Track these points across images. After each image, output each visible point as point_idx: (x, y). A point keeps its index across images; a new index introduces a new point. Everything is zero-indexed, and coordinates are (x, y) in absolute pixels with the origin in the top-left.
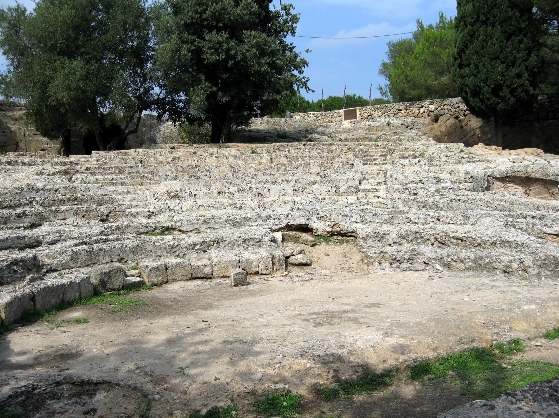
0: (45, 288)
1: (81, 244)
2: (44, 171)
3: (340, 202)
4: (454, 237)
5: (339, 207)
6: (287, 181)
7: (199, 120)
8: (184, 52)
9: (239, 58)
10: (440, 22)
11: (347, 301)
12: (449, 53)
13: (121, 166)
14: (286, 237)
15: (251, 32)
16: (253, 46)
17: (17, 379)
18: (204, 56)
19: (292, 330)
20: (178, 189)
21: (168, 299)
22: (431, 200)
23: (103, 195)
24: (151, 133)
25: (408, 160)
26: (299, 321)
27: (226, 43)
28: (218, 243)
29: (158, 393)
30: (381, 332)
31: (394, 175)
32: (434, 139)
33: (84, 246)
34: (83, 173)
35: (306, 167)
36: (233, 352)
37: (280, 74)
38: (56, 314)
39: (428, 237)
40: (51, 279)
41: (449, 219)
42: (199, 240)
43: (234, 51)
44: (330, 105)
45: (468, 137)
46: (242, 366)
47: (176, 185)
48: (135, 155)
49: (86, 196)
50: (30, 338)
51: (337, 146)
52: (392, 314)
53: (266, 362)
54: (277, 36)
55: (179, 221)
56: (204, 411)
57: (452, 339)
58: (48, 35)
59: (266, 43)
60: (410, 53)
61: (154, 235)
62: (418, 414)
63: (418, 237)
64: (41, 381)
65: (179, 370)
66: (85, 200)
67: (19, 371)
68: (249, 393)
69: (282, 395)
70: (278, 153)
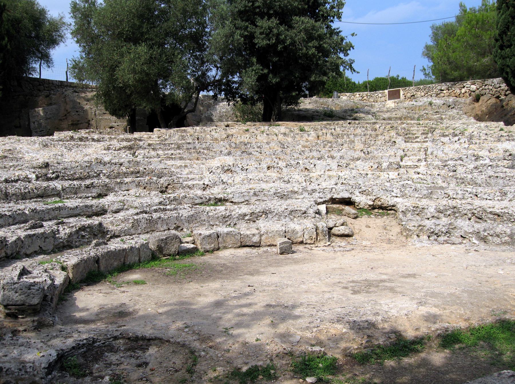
0: (108, 252)
1: (142, 212)
2: (111, 147)
3: (382, 178)
4: (491, 213)
5: (380, 182)
6: (333, 157)
7: (252, 100)
8: (237, 37)
9: (288, 42)
10: (483, 5)
11: (385, 271)
12: (491, 35)
13: (180, 142)
14: (330, 210)
15: (300, 17)
16: (301, 31)
17: (80, 332)
18: (256, 41)
19: (330, 297)
20: (231, 164)
21: (219, 264)
22: (470, 176)
23: (162, 169)
24: (209, 112)
25: (448, 138)
26: (338, 289)
27: (276, 28)
28: (266, 214)
29: (204, 351)
30: (415, 301)
31: (434, 152)
32: (475, 118)
33: (144, 215)
34: (145, 148)
35: (351, 144)
36: (274, 315)
37: (327, 57)
38: (117, 276)
39: (466, 211)
40: (114, 244)
41: (486, 195)
42: (249, 211)
43: (283, 36)
44: (375, 86)
45: (508, 116)
46: (282, 328)
47: (229, 160)
48: (192, 133)
49: (147, 169)
50: (93, 296)
51: (380, 125)
52: (427, 285)
53: (305, 325)
54: (324, 21)
55: (231, 194)
56: (245, 369)
57: (485, 311)
58: (116, 23)
59: (313, 28)
60: (452, 35)
61: (208, 205)
62: (447, 381)
63: (455, 212)
64: (100, 336)
65: (224, 330)
66: (147, 173)
67: (82, 325)
68: (287, 354)
69: (318, 357)
70: (324, 131)
